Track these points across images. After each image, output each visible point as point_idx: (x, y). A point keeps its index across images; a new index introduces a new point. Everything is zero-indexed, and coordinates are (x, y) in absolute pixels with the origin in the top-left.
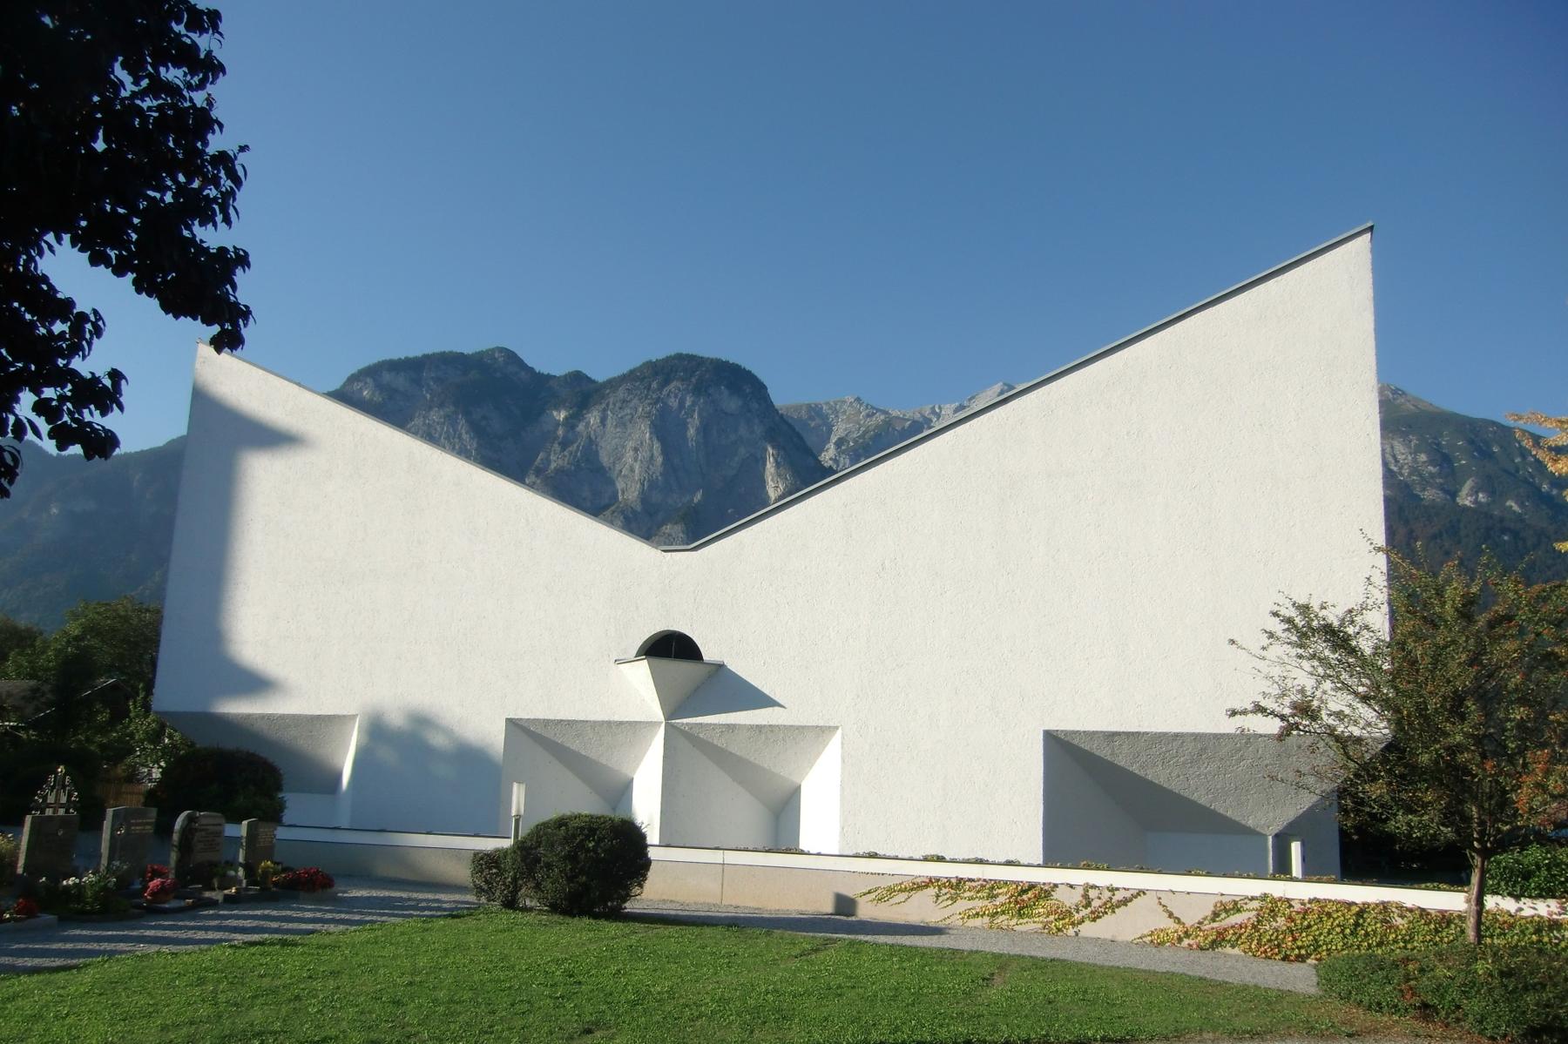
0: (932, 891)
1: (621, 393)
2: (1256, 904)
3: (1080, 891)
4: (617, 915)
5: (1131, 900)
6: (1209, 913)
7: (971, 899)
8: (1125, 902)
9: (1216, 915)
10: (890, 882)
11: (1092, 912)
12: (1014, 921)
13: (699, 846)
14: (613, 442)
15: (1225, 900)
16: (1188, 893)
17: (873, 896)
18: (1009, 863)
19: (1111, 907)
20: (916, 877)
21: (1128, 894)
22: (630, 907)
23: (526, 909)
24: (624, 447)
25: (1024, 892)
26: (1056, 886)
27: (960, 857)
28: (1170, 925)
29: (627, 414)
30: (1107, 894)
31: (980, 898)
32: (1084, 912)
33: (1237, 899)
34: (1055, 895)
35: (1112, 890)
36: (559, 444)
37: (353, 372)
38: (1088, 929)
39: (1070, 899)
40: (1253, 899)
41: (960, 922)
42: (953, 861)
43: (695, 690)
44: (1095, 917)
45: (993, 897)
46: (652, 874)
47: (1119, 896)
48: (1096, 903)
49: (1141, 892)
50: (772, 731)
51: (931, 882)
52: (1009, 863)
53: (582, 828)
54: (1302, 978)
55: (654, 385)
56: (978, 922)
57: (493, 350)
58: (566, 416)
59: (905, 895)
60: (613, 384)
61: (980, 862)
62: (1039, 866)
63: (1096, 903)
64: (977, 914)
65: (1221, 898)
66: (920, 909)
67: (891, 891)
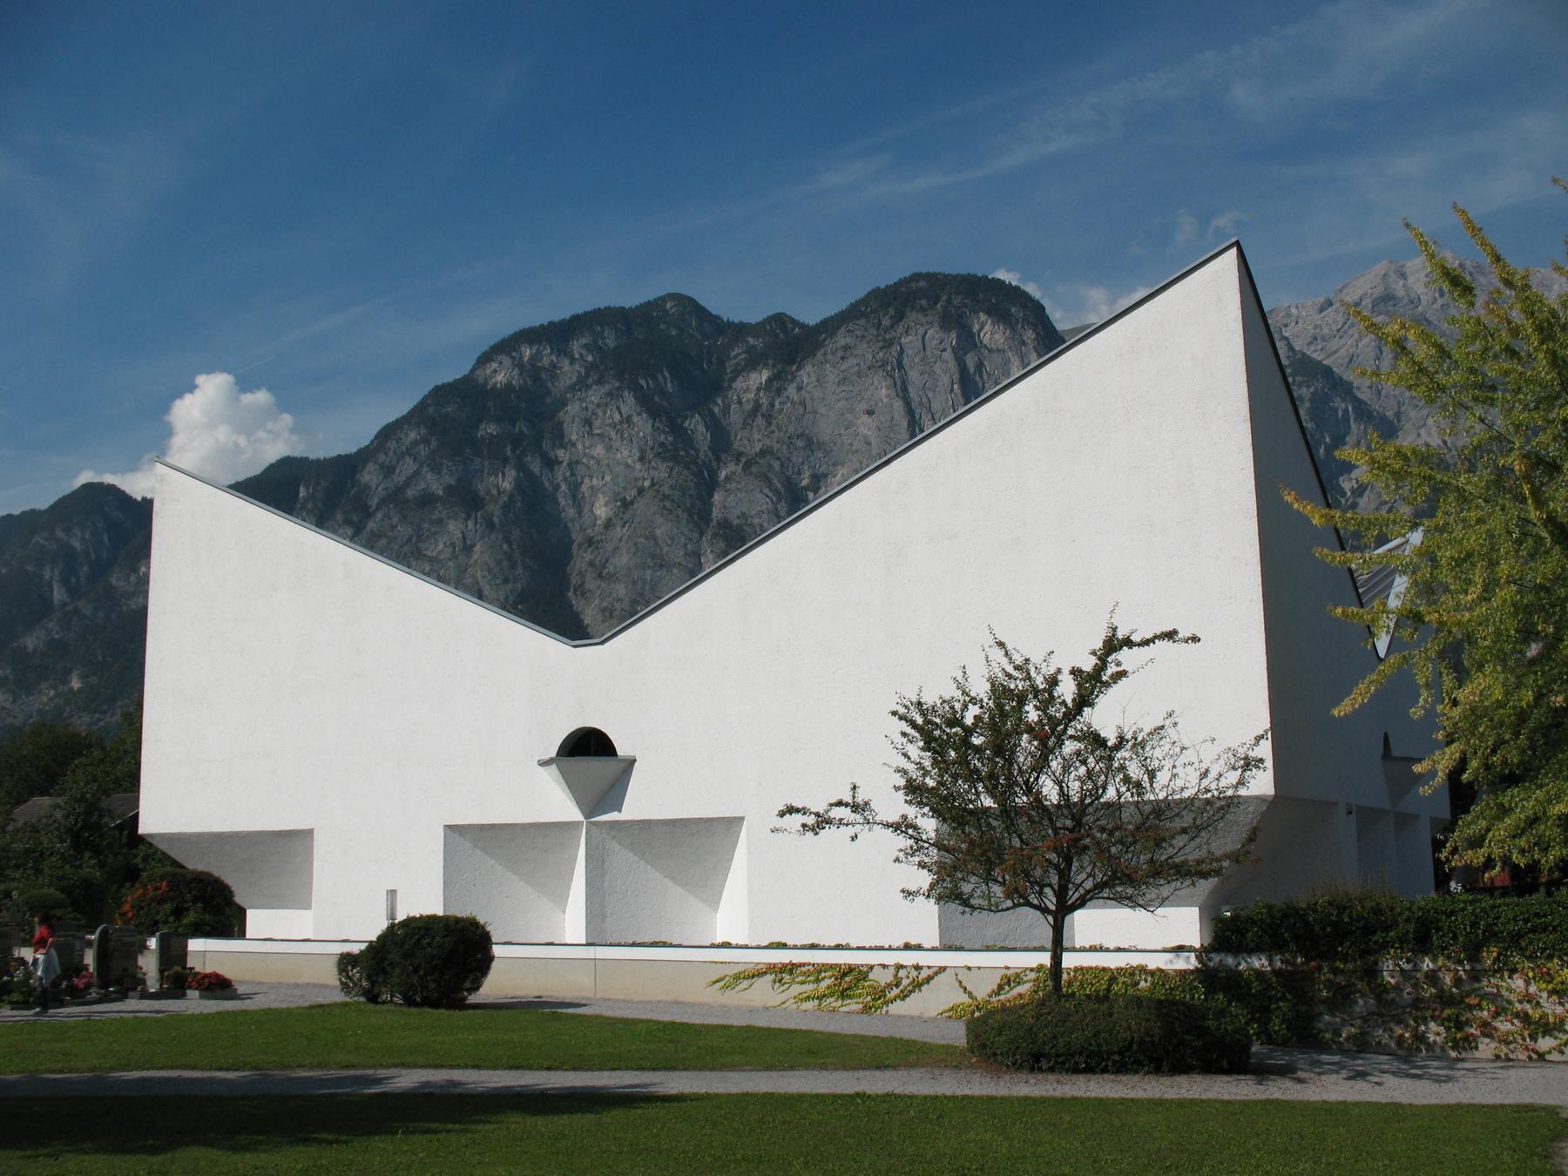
0: (770, 977)
1: (842, 339)
2: (1033, 975)
3: (892, 970)
4: (461, 1005)
5: (933, 978)
6: (995, 987)
7: (802, 983)
8: (929, 979)
9: (1000, 987)
10: (737, 970)
11: (902, 992)
12: (840, 1002)
13: (524, 942)
14: (837, 406)
15: (1009, 972)
16: (979, 968)
17: (722, 983)
18: (838, 947)
19: (917, 985)
20: (758, 964)
21: (930, 972)
22: (473, 999)
23: (384, 1002)
24: (851, 410)
25: (845, 974)
26: (872, 967)
27: (799, 944)
28: (965, 999)
29: (852, 367)
30: (914, 973)
31: (810, 982)
32: (895, 991)
33: (1019, 971)
34: (871, 976)
35: (918, 968)
36: (763, 416)
37: (483, 350)
38: (897, 1008)
39: (882, 978)
40: (1032, 970)
41: (795, 1006)
42: (795, 947)
43: (611, 788)
44: (904, 996)
45: (818, 981)
46: (494, 965)
47: (924, 974)
48: (905, 982)
49: (942, 969)
50: (685, 826)
51: (771, 968)
52: (838, 947)
53: (420, 928)
54: (1300, 1074)
55: (886, 322)
56: (810, 1005)
57: (664, 299)
58: (769, 377)
59: (750, 981)
60: (830, 326)
61: (813, 947)
62: (933, 949)
63: (905, 982)
64: (808, 997)
65: (1005, 971)
66: (763, 994)
67: (738, 978)
